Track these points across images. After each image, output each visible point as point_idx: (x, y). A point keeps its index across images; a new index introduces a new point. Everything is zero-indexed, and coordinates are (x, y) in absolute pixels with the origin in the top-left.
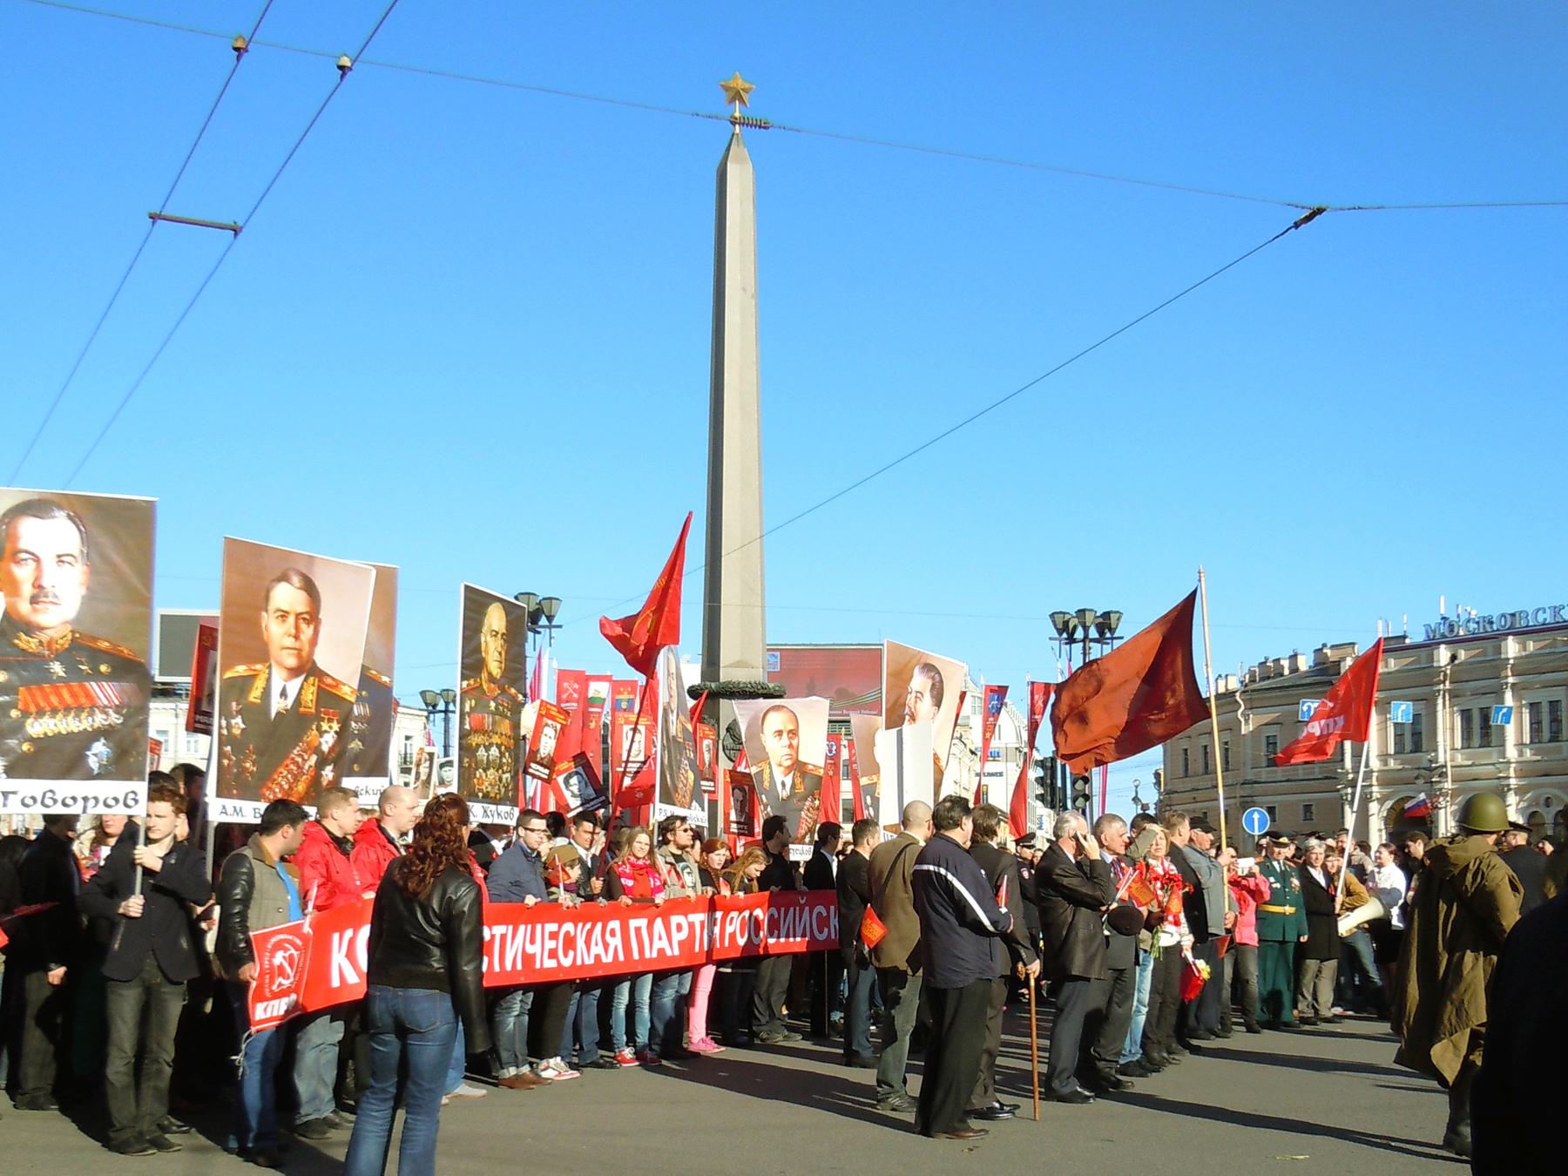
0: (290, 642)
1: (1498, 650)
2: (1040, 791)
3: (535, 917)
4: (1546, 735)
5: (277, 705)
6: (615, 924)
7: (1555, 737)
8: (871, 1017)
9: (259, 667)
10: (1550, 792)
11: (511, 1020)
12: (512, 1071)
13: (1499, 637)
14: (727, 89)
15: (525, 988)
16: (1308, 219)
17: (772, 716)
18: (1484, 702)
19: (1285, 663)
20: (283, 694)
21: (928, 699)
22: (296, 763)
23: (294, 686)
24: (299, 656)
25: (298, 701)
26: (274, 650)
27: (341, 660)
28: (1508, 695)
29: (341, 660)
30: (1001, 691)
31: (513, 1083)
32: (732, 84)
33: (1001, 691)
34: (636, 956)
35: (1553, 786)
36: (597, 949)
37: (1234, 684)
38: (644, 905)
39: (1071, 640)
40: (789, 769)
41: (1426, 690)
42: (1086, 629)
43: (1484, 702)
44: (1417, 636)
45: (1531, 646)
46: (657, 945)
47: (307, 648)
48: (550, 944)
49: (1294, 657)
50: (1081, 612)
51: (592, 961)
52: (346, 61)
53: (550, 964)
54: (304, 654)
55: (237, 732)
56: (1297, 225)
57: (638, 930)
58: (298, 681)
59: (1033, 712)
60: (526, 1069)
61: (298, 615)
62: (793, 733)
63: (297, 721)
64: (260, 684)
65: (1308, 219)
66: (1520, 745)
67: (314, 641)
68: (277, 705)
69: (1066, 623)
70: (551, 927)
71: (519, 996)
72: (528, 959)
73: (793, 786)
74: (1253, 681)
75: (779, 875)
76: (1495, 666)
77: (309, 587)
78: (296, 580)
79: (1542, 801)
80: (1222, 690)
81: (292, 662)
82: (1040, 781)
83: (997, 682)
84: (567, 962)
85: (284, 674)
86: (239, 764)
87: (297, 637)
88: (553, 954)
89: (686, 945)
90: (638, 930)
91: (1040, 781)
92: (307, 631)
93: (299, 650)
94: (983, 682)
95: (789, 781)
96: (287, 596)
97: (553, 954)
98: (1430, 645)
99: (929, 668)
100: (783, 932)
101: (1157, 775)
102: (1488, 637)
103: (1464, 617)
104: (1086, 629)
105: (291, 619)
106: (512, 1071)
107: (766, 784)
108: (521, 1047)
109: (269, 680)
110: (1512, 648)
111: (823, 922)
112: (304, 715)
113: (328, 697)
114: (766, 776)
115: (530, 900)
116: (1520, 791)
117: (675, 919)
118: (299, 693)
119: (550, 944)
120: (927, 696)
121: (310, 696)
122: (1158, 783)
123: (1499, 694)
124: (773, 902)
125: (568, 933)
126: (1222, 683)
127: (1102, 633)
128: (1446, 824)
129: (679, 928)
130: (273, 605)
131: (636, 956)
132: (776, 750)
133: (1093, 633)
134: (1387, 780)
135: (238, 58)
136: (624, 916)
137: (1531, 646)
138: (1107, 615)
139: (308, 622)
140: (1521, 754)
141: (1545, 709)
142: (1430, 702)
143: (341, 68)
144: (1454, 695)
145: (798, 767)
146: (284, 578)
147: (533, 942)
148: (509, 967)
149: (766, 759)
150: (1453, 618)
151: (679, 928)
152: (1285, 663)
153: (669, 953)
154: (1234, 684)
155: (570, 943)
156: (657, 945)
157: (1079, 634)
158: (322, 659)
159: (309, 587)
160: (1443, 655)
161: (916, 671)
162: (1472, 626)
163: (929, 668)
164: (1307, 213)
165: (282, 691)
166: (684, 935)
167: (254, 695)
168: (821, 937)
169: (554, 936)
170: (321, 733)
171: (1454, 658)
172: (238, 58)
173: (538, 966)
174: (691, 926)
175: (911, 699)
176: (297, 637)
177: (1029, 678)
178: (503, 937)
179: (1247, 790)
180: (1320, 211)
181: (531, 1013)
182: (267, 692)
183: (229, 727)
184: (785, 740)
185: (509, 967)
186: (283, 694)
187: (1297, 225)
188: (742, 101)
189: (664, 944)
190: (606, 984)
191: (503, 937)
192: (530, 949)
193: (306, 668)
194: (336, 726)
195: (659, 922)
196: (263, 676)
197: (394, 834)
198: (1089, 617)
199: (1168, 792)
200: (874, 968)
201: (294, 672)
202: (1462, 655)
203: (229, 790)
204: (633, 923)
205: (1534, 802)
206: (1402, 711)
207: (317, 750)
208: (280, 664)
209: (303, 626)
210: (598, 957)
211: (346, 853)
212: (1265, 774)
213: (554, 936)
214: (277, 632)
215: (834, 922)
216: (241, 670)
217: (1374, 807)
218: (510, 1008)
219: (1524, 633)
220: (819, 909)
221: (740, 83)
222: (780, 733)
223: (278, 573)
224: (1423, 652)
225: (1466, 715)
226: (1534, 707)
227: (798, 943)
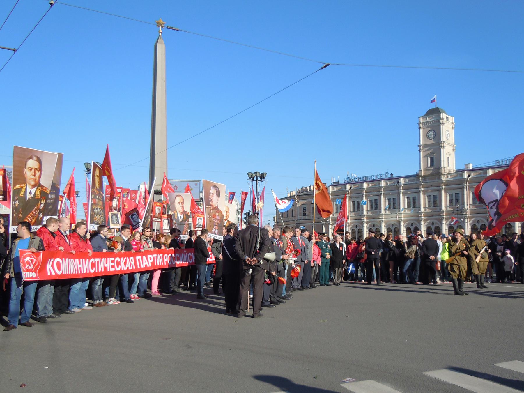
0: (32, 177)
1: (379, 184)
2: (245, 221)
3: (106, 256)
4: (374, 208)
5: (28, 196)
6: (132, 258)
7: (376, 209)
8: (205, 284)
9: (23, 185)
10: (479, 219)
11: (97, 287)
12: (98, 302)
13: (362, 183)
14: (158, 23)
15: (102, 277)
16: (325, 67)
17: (177, 198)
18: (359, 199)
19: (308, 188)
20: (30, 193)
21: (215, 195)
22: (33, 213)
23: (33, 191)
24: (35, 181)
25: (35, 195)
26: (28, 180)
27: (46, 182)
28: (364, 198)
29: (46, 182)
30: (233, 194)
31: (98, 305)
32: (159, 22)
33: (233, 194)
34: (139, 267)
35: (483, 217)
36: (128, 265)
37: (295, 193)
38: (138, 252)
39: (253, 180)
40: (182, 213)
41: (460, 186)
42: (257, 177)
43: (359, 199)
44: (341, 182)
45: (370, 185)
46: (144, 264)
47: (38, 179)
48: (113, 264)
49: (310, 187)
50: (256, 173)
51: (126, 269)
52: (52, 2)
53: (113, 269)
54: (37, 180)
55: (17, 205)
56: (322, 68)
57: (139, 259)
58: (35, 189)
59: (242, 200)
60: (102, 301)
61: (35, 169)
62: (183, 203)
63: (35, 200)
64: (23, 190)
65: (325, 67)
66: (367, 211)
67: (40, 177)
68: (28, 196)
69: (252, 176)
70: (112, 259)
71: (99, 280)
72: (105, 268)
73: (183, 218)
74: (300, 193)
75: (176, 243)
76: (361, 190)
77: (39, 161)
78: (35, 158)
79: (476, 221)
80: (292, 195)
81: (33, 183)
82: (245, 218)
83: (232, 191)
84: (118, 269)
85: (31, 187)
86: (17, 215)
87: (35, 175)
88: (113, 267)
89: (153, 263)
90: (139, 259)
91: (245, 218)
92: (38, 174)
93: (35, 179)
94: (228, 191)
95: (182, 216)
96: (32, 163)
97: (113, 267)
98: (345, 184)
99: (215, 187)
100: (181, 260)
101: (274, 218)
102: (360, 183)
103: (353, 177)
104: (257, 177)
105: (33, 170)
106: (98, 302)
107: (176, 217)
108: (100, 295)
109: (26, 189)
110: (383, 184)
111: (191, 258)
112: (37, 199)
113: (44, 194)
114: (176, 215)
115: (104, 251)
116: (367, 223)
117: (149, 256)
118: (35, 192)
119: (113, 264)
120: (215, 194)
121: (38, 193)
122: (274, 220)
123: (362, 197)
124: (175, 252)
125: (117, 261)
126: (291, 193)
127: (261, 179)
128: (199, 233)
129: (151, 259)
130: (27, 166)
131: (139, 267)
132: (178, 207)
133: (259, 179)
134: (426, 215)
135: (51, 7)
136: (134, 255)
137: (370, 185)
138: (263, 174)
139: (39, 171)
140: (367, 213)
141: (373, 201)
142: (344, 199)
143: (51, 4)
144: (351, 198)
145: (184, 212)
146: (31, 158)
147: (106, 263)
148: (100, 271)
149: (176, 210)
150: (351, 177)
151: (151, 259)
152: (308, 188)
153: (148, 266)
154: (295, 193)
155: (119, 264)
156: (144, 264)
157: (255, 179)
158: (42, 182)
159: (39, 161)
160: (348, 187)
161: (211, 188)
162: (355, 179)
163: (215, 187)
164: (325, 65)
165: (30, 192)
166: (152, 260)
167: (22, 194)
168: (191, 262)
169: (113, 261)
170: (41, 204)
171: (351, 188)
172: (51, 7)
173: (108, 270)
174: (154, 258)
175: (210, 196)
176: (35, 175)
177: (241, 191)
178: (98, 262)
179: (298, 222)
180: (328, 65)
181: (103, 285)
182: (25, 192)
183: (15, 204)
184: (181, 205)
185: (100, 271)
186: (30, 193)
187: (322, 68)
188: (162, 27)
189: (147, 263)
190: (131, 276)
191: (98, 262)
192: (106, 265)
193: (38, 185)
194: (44, 201)
195: (144, 257)
196: (24, 188)
197: (63, 232)
198: (258, 174)
199: (277, 222)
200: (223, 274)
201: (34, 186)
202: (353, 187)
203: (15, 223)
204: (137, 258)
205: (370, 225)
206: (339, 201)
207: (39, 209)
208: (30, 184)
209: (37, 172)
210: (128, 268)
211: (54, 237)
212: (302, 218)
213: (113, 261)
214: (29, 174)
215: (194, 257)
216: (18, 186)
217: (330, 227)
218: (97, 284)
219: (369, 182)
220: (190, 254)
221: (161, 22)
222: (179, 203)
223: (29, 156)
224: (343, 186)
225: (354, 203)
226: (389, 200)
227: (185, 264)
